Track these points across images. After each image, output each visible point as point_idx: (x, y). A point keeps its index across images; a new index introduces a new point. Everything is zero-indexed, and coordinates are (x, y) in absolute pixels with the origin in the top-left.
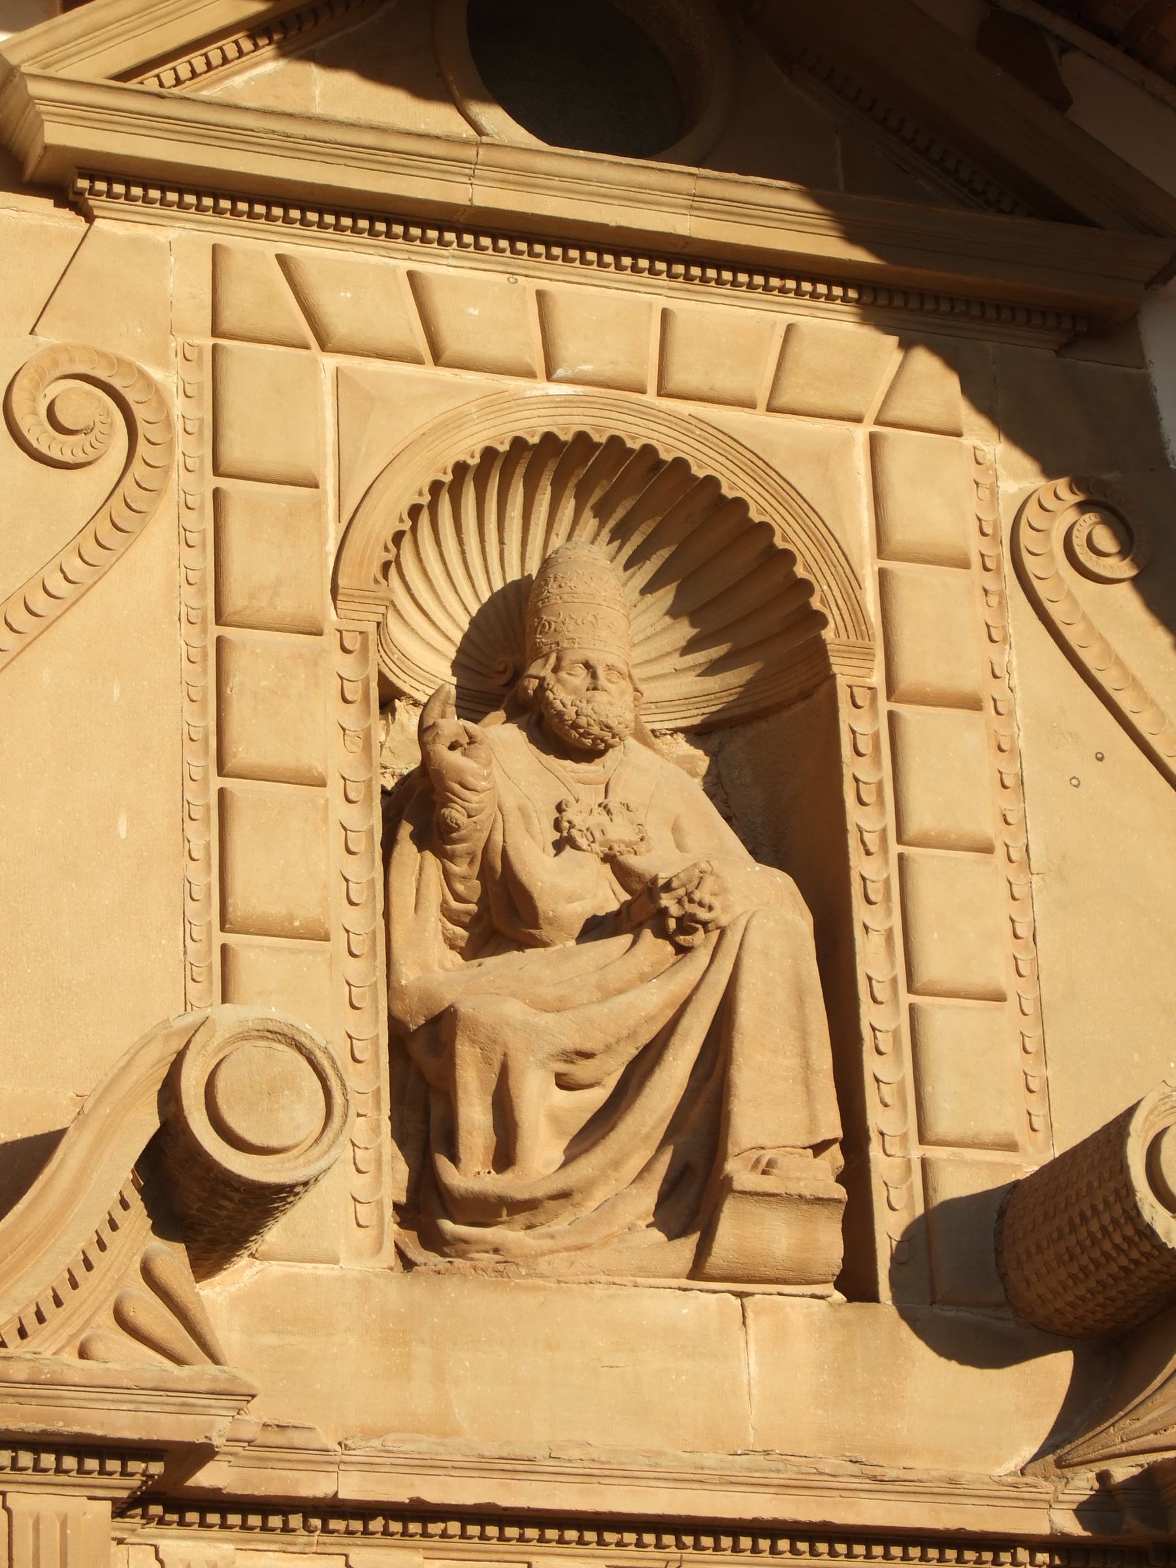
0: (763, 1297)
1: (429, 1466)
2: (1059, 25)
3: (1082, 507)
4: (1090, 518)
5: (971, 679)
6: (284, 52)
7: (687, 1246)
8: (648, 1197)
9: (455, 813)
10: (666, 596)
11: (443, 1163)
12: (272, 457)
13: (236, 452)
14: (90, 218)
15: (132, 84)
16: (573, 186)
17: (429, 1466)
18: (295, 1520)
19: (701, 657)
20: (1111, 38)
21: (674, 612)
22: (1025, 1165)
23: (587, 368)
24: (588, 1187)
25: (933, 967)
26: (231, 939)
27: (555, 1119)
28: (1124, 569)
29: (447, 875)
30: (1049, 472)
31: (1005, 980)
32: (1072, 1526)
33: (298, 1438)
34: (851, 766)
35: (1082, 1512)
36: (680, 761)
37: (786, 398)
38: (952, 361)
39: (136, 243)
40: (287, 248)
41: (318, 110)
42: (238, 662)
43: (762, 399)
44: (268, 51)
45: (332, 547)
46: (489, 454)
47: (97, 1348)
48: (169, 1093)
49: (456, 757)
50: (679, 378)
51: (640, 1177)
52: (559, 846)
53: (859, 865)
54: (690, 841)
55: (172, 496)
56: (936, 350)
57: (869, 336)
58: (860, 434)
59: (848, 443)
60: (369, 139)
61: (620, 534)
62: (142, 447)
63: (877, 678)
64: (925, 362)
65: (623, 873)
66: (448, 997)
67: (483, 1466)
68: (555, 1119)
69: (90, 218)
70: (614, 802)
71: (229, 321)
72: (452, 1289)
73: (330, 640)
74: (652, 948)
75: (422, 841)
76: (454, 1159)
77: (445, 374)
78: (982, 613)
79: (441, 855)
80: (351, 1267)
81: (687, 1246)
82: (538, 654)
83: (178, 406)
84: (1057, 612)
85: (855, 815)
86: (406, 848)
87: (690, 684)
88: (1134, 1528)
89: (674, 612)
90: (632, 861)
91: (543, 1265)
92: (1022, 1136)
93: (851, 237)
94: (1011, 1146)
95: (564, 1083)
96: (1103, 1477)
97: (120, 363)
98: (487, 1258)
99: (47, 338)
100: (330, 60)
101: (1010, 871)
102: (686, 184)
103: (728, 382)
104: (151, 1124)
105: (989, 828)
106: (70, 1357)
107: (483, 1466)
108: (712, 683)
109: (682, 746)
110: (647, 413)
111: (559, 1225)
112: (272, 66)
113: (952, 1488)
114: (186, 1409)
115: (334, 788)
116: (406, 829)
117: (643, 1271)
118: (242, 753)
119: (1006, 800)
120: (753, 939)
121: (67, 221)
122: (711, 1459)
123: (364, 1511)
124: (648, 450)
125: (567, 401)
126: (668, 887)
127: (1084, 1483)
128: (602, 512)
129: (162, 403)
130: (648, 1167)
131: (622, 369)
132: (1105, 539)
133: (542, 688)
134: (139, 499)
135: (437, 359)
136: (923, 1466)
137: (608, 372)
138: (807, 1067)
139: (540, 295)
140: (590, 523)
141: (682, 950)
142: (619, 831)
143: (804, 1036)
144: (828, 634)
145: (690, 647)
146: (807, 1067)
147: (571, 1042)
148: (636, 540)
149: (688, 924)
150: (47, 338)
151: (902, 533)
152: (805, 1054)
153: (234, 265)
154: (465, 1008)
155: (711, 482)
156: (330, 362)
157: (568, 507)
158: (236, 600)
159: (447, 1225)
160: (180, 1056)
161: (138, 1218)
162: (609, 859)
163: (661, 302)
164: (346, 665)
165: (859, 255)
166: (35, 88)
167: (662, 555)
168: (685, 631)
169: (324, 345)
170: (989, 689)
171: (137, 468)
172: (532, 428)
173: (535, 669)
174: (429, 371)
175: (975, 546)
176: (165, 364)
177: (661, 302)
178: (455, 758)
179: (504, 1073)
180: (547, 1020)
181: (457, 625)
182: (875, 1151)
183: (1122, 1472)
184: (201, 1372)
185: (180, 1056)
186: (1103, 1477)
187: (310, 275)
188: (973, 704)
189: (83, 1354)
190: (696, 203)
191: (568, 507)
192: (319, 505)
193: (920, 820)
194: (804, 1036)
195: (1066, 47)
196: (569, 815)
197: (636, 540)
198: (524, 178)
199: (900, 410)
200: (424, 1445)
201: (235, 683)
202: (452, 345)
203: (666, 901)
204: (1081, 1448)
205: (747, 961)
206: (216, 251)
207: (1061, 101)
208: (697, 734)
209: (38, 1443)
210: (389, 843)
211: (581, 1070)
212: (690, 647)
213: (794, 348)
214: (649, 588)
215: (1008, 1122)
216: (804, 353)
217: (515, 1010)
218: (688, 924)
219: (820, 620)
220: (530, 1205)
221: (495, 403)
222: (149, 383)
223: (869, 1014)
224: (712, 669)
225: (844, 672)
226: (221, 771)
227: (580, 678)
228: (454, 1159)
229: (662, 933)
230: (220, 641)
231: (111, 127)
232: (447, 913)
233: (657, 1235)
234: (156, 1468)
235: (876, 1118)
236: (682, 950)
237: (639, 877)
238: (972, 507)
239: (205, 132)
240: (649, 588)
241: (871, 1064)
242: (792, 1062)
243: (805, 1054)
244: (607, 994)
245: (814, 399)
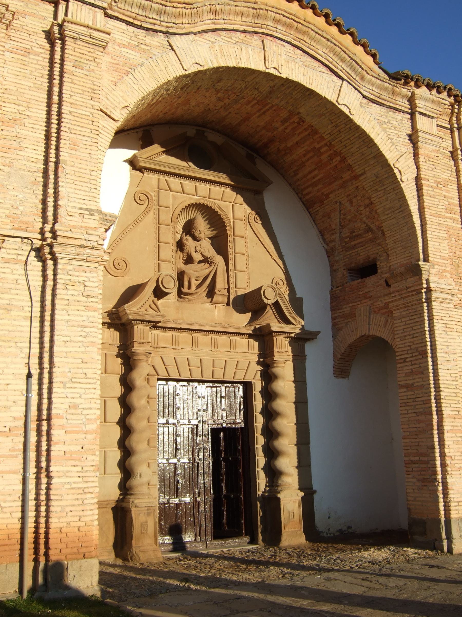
0: (218, 305)
1: (182, 324)
2: (255, 155)
3: (256, 214)
4: (257, 216)
5: (243, 234)
6: (166, 154)
7: (210, 299)
8: (205, 293)
9: (185, 248)
10: (207, 222)
11: (182, 288)
12: (165, 204)
13: (161, 204)
14: (144, 174)
15: (149, 158)
16: (200, 173)
17: (182, 324)
18: (167, 329)
19: (211, 229)
20: (261, 157)
21: (208, 224)
22: (247, 291)
23: (201, 195)
24: (199, 292)
25: (238, 268)
26: (159, 262)
27: (195, 284)
28: (260, 222)
29: (183, 255)
30: (252, 210)
31: (246, 270)
32: (251, 333)
33: (168, 320)
34: (229, 244)
35: (252, 331)
36: (208, 241)
37: (223, 200)
38: (242, 196)
39: (149, 177)
40: (166, 179)
41: (170, 162)
42: (161, 229)
43: (220, 199)
44: (164, 154)
45: (171, 215)
46: (189, 205)
47: (148, 310)
48: (157, 282)
49: (185, 241)
50: (211, 197)
51: (204, 291)
52: (195, 252)
53: (230, 256)
54: (210, 251)
55: (153, 209)
56: (240, 195)
57: (232, 192)
58: (231, 204)
59: (230, 205)
60: (177, 166)
61: (202, 214)
62: (150, 203)
63: (232, 234)
64: (239, 196)
65: (203, 256)
66: (183, 269)
67: (188, 324)
68: (195, 284)
69: (144, 174)
70: (202, 246)
71: (160, 187)
72: (184, 303)
73: (171, 227)
74: (207, 265)
75: (180, 251)
76: (183, 288)
77: (184, 195)
78: (244, 226)
79: (183, 253)
80: (173, 301)
81: (210, 299)
82: (193, 229)
83: (154, 197)
84: (253, 227)
85: (229, 250)
86: (179, 252)
87: (209, 232)
88: (258, 333)
89: (208, 224)
90: (204, 254)
91: (194, 301)
92: (247, 288)
93: (232, 181)
94: (245, 289)
95: (196, 280)
96: (255, 327)
97: (147, 192)
98: (187, 300)
99: (139, 189)
100: (172, 155)
101: (246, 257)
102: (213, 174)
103: (216, 197)
104: (155, 285)
105: (244, 252)
106: (145, 311)
107: (188, 324)
108: (212, 232)
109: (208, 240)
110: (207, 201)
111: (195, 296)
112: (165, 156)
113: (239, 328)
114: (159, 317)
115: (171, 245)
116: (179, 249)
117: (205, 302)
118: (161, 240)
119: (246, 249)
120: (219, 265)
121: (141, 174)
122: (213, 324)
123: (174, 328)
124: (207, 205)
125: (198, 199)
126: (209, 258)
127: (253, 328)
128: (200, 212)
129: (152, 197)
130: (205, 290)
131: (205, 195)
132: (258, 218)
133: (194, 233)
134: (149, 209)
135: (183, 193)
136: (235, 325)
137: (203, 195)
138: (224, 279)
139: (195, 186)
140: (199, 213)
141: (210, 265)
142: (202, 250)
143: (224, 276)
144: (227, 228)
145: (209, 228)
146: (224, 279)
147: (198, 276)
148: (204, 215)
149: (211, 262)
150: (139, 189)
151: (236, 216)
152: (224, 278)
153: (161, 181)
154: (186, 271)
155: (214, 209)
156: (171, 193)
157: (197, 211)
158: (161, 222)
159: (182, 296)
160: (159, 278)
161: (152, 296)
162: (201, 254)
163: (209, 187)
164: (172, 230)
165: (232, 183)
166: (139, 158)
167: (206, 214)
168: (209, 226)
169: (171, 191)
170: (245, 235)
171: (149, 205)
172: (194, 202)
173: (193, 230)
174: (182, 194)
175: (244, 218)
176: (152, 192)
177: (209, 187)
178: (185, 241)
179: (190, 279)
180: (195, 273)
181: (183, 224)
182: (230, 289)
183: (257, 327)
184: (159, 313)
185: (159, 278)
186: (255, 327)
187: (169, 182)
188: (243, 237)
189: (146, 311)
190: (214, 176)
191: (197, 211)
192: (170, 210)
193: (237, 251)
194: (224, 276)
195: (256, 158)
196: (197, 248)
197: (204, 215)
198: (195, 172)
199: (236, 202)
200: (182, 321)
201: (160, 232)
202: (185, 191)
203: (209, 260)
204: (252, 324)
205: (218, 267)
206: (158, 179)
207: (255, 164)
208: (210, 238)
209: (141, 321)
210: (177, 251)
211: (198, 279)
212: (209, 228)
213: (224, 193)
214: (205, 221)
215: (246, 286)
216: (226, 194)
217: (191, 271)
218: (211, 262)
219: (226, 226)
220: (192, 294)
221: (190, 199)
222: (151, 195)
223: (230, 273)
224: (212, 231)
225: (229, 233)
226: (159, 242)
227: (198, 232)
228: (183, 288)
229: (208, 263)
230: (158, 227)
231: (147, 163)
232: (183, 259)
233: (206, 298)
234: (154, 324)
235: (231, 285)
236: (210, 265)
237: (205, 256)
238: (244, 213)
239: (158, 165)
240: (205, 221)
241: (230, 279)
242: (223, 279)
243: (224, 278)
244: (202, 270)
245: (226, 200)
